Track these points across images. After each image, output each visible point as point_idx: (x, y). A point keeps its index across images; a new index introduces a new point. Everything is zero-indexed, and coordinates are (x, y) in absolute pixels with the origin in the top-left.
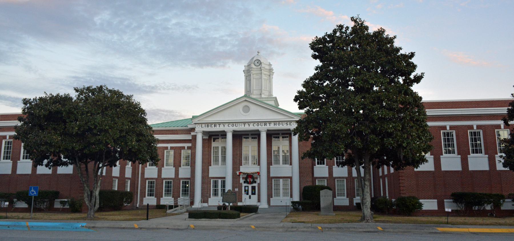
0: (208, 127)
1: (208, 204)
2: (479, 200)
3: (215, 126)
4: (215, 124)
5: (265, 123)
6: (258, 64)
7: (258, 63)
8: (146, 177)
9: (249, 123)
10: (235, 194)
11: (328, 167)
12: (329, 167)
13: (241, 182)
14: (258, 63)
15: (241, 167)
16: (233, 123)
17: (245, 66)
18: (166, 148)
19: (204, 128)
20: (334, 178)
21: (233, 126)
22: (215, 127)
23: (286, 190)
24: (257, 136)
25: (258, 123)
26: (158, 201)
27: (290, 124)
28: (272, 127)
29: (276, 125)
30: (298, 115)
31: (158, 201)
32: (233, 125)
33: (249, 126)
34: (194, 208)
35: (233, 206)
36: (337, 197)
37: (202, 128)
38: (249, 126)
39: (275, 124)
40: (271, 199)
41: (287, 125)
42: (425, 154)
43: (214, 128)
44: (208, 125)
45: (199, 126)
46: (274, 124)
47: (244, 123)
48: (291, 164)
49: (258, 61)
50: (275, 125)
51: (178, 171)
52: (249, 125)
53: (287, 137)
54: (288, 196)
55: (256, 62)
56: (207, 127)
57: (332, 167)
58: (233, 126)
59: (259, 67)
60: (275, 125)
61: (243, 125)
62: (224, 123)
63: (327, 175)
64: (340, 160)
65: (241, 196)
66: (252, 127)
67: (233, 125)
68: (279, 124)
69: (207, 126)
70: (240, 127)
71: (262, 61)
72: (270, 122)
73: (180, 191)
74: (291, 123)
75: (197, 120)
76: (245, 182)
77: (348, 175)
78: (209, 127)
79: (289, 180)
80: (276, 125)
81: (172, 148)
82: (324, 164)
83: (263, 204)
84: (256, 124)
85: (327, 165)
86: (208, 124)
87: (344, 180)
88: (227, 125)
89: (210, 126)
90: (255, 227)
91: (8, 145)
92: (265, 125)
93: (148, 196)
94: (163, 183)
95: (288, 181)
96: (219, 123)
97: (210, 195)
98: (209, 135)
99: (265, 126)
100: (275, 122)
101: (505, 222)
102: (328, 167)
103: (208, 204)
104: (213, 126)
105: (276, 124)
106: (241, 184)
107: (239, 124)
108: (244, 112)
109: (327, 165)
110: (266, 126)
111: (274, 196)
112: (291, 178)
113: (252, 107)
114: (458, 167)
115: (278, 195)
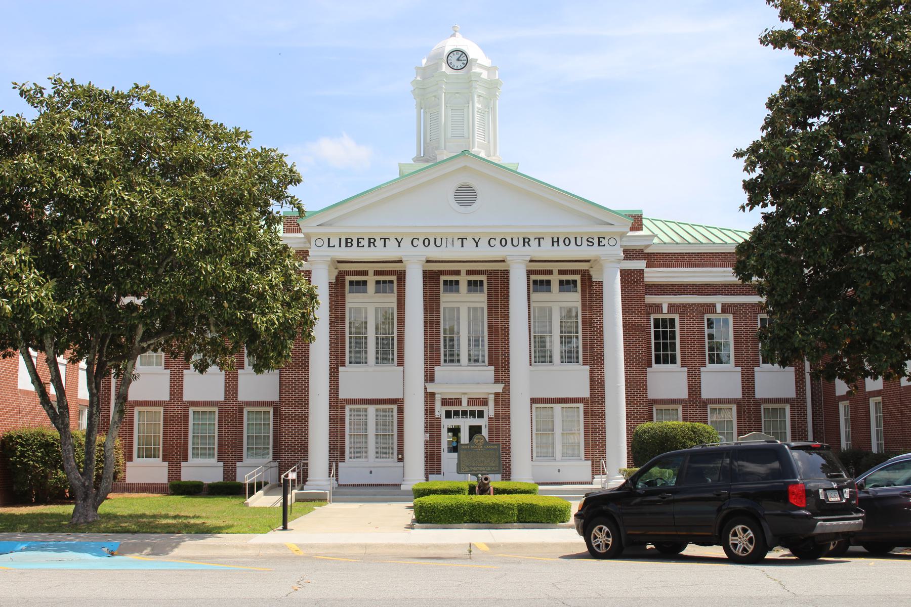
0: (349, 245)
1: (337, 480)
2: (81, 464)
3: (370, 242)
6: (459, 64)
7: (458, 60)
8: (342, 396)
10: (496, 447)
11: (686, 369)
12: (688, 371)
13: (439, 414)
14: (458, 60)
15: (436, 368)
18: (711, 308)
20: (704, 402)
21: (503, 243)
22: (369, 246)
23: (359, 437)
24: (394, 278)
29: (558, 245)
36: (192, 461)
40: (183, 464)
41: (591, 244)
42: (216, 338)
46: (553, 242)
48: (401, 363)
50: (556, 244)
51: (236, 379)
54: (159, 457)
55: (453, 58)
56: (346, 246)
57: (699, 370)
58: (503, 243)
60: (556, 244)
63: (684, 394)
65: (439, 456)
71: (471, 56)
73: (241, 442)
76: (448, 415)
77: (743, 394)
78: (352, 245)
79: (395, 407)
80: (558, 245)
81: (726, 308)
82: (673, 361)
85: (683, 366)
87: (784, 409)
93: (139, 457)
94: (187, 416)
95: (675, 412)
97: (343, 453)
98: (337, 270)
99: (524, 245)
102: (686, 369)
105: (558, 242)
106: (439, 419)
109: (683, 366)
111: (350, 458)
112: (399, 403)
114: (190, 376)
115: (360, 452)
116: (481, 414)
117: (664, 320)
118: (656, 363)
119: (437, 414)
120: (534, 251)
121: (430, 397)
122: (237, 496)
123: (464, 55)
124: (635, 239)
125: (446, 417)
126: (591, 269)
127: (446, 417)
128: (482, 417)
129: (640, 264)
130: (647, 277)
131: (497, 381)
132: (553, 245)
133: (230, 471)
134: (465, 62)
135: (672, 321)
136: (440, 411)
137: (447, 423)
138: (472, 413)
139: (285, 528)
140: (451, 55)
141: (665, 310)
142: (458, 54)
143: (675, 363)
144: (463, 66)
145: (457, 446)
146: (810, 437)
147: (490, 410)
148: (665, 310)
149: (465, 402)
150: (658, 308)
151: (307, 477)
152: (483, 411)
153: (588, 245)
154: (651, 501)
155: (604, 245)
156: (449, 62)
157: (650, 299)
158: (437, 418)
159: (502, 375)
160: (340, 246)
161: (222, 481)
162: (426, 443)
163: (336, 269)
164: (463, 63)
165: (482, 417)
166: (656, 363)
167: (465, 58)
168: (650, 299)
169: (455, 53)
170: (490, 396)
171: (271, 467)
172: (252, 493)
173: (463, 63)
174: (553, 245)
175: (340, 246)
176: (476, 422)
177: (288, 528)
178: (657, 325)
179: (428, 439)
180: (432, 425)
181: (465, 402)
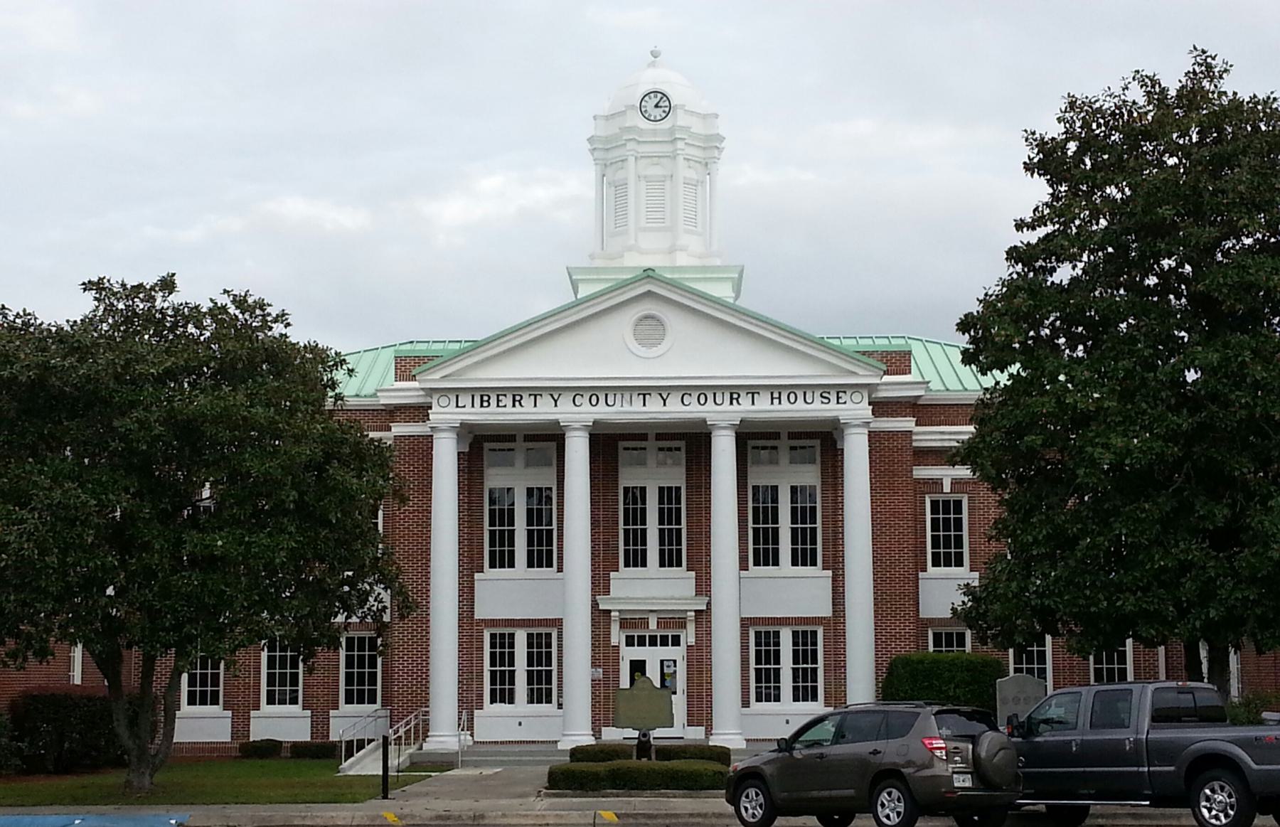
1: (472, 735)
4: (517, 394)
5: (734, 393)
6: (658, 113)
7: (656, 106)
9: (663, 392)
14: (656, 106)
16: (595, 393)
17: (595, 118)
19: (468, 409)
21: (702, 402)
22: (514, 406)
25: (704, 392)
26: (241, 725)
27: (838, 398)
28: (763, 409)
29: (780, 403)
30: (864, 358)
31: (241, 725)
32: (594, 398)
33: (665, 405)
34: (429, 754)
35: (597, 745)
36: (265, 708)
37: (459, 410)
38: (665, 405)
39: (776, 395)
41: (826, 401)
43: (509, 409)
44: (486, 398)
45: (444, 401)
47: (644, 392)
49: (659, 96)
50: (776, 401)
52: (665, 401)
53: (678, 449)
56: (482, 406)
58: (702, 402)
59: (666, 124)
60: (776, 401)
61: (638, 401)
62: (555, 393)
64: (811, 549)
66: (676, 410)
67: (594, 398)
68: (792, 398)
69: (482, 401)
70: (627, 408)
72: (753, 391)
74: (501, 398)
75: (437, 376)
76: (630, 642)
78: (489, 405)
80: (780, 403)
83: (717, 732)
84: (695, 395)
86: (483, 395)
88: (680, 399)
89: (493, 401)
90: (618, 816)
91: (538, 505)
92: (732, 399)
96: (536, 393)
98: (471, 435)
99: (731, 403)
100: (776, 391)
101: (876, 752)
103: (472, 735)
104: (507, 401)
105: (780, 398)
107: (619, 396)
108: (654, 345)
110: (735, 406)
113: (673, 319)
116: (676, 641)
117: (946, 503)
118: (934, 565)
119: (614, 641)
120: (746, 408)
121: (600, 618)
122: (1211, 751)
123: (665, 98)
124: (894, 386)
125: (627, 645)
126: (834, 432)
127: (627, 645)
128: (679, 645)
129: (907, 423)
130: (916, 440)
131: (699, 592)
132: (772, 403)
133: (320, 724)
134: (667, 109)
135: (958, 504)
136: (617, 636)
137: (630, 654)
138: (664, 642)
139: (385, 797)
140: (647, 98)
141: (947, 488)
142: (656, 97)
143: (679, 645)
144: (664, 115)
145: (281, 758)
146: (1162, 676)
147: (689, 636)
148: (947, 488)
149: (653, 624)
150: (936, 484)
151: (428, 731)
152: (679, 636)
153: (822, 402)
154: (502, 761)
155: (845, 403)
156: (643, 110)
157: (922, 472)
158: (613, 646)
159: (703, 586)
160: (473, 406)
161: (309, 739)
162: (595, 684)
163: (470, 433)
164: (664, 112)
165: (679, 645)
166: (934, 565)
167: (667, 103)
168: (922, 472)
169: (652, 95)
170: (689, 613)
171: (379, 717)
172: (350, 754)
173: (664, 112)
174: (772, 403)
175: (473, 406)
176: (669, 652)
177: (389, 797)
178: (935, 509)
179: (601, 676)
180: (603, 655)
181: (653, 624)
